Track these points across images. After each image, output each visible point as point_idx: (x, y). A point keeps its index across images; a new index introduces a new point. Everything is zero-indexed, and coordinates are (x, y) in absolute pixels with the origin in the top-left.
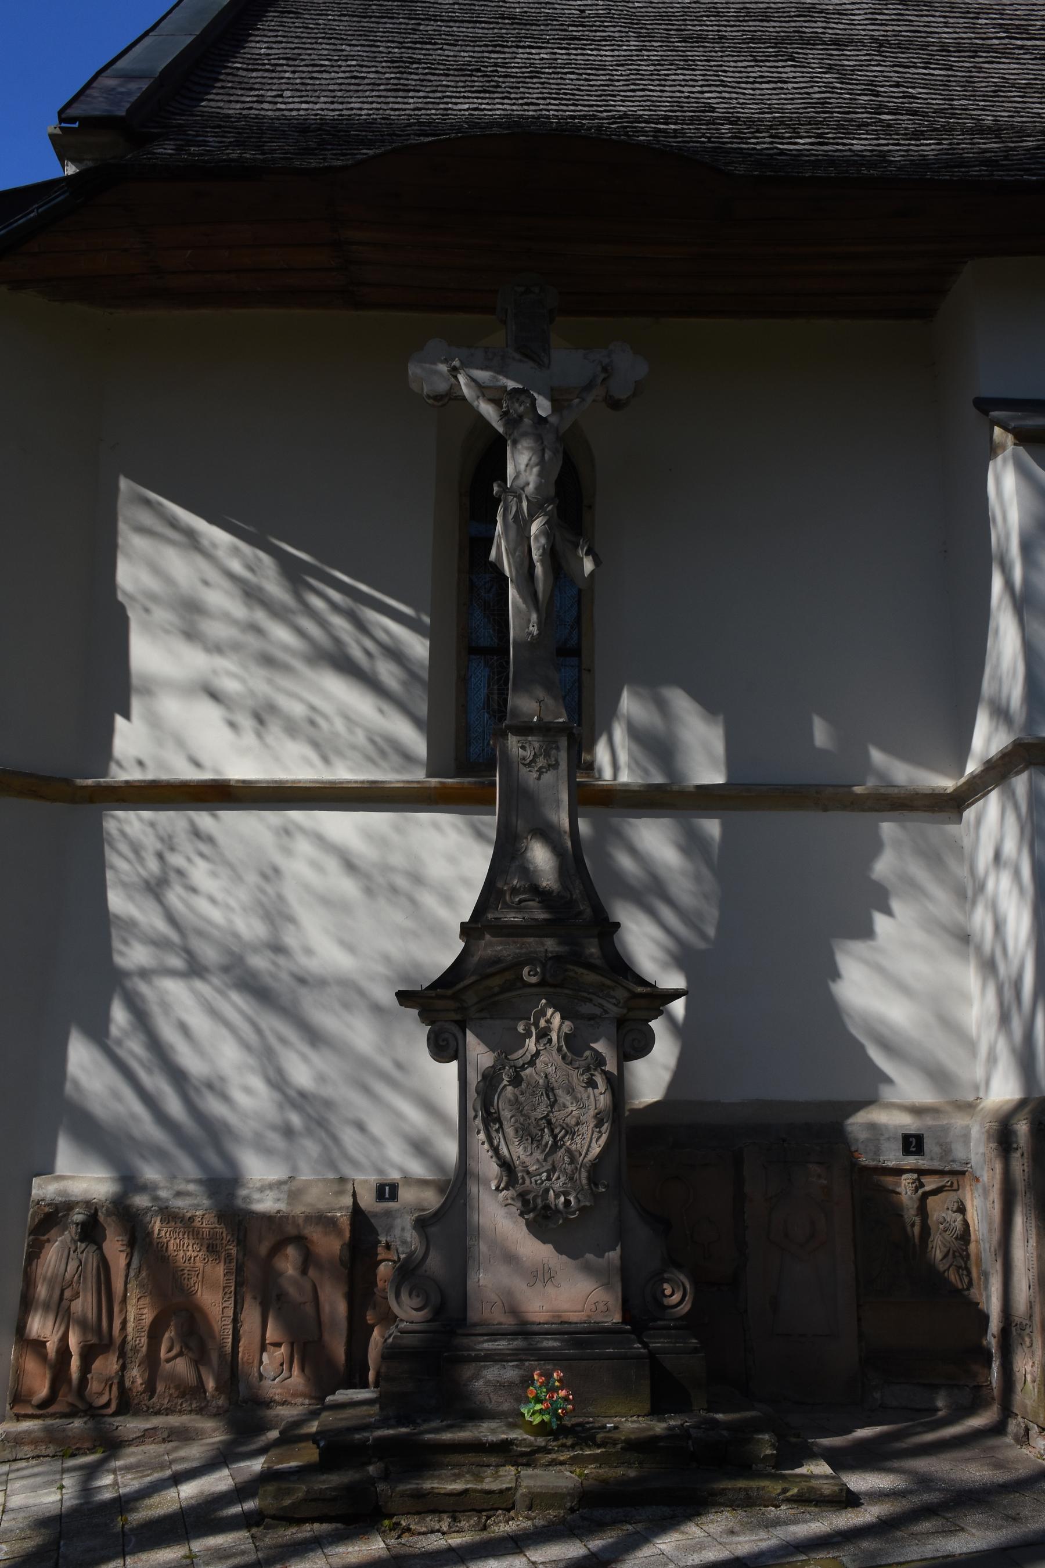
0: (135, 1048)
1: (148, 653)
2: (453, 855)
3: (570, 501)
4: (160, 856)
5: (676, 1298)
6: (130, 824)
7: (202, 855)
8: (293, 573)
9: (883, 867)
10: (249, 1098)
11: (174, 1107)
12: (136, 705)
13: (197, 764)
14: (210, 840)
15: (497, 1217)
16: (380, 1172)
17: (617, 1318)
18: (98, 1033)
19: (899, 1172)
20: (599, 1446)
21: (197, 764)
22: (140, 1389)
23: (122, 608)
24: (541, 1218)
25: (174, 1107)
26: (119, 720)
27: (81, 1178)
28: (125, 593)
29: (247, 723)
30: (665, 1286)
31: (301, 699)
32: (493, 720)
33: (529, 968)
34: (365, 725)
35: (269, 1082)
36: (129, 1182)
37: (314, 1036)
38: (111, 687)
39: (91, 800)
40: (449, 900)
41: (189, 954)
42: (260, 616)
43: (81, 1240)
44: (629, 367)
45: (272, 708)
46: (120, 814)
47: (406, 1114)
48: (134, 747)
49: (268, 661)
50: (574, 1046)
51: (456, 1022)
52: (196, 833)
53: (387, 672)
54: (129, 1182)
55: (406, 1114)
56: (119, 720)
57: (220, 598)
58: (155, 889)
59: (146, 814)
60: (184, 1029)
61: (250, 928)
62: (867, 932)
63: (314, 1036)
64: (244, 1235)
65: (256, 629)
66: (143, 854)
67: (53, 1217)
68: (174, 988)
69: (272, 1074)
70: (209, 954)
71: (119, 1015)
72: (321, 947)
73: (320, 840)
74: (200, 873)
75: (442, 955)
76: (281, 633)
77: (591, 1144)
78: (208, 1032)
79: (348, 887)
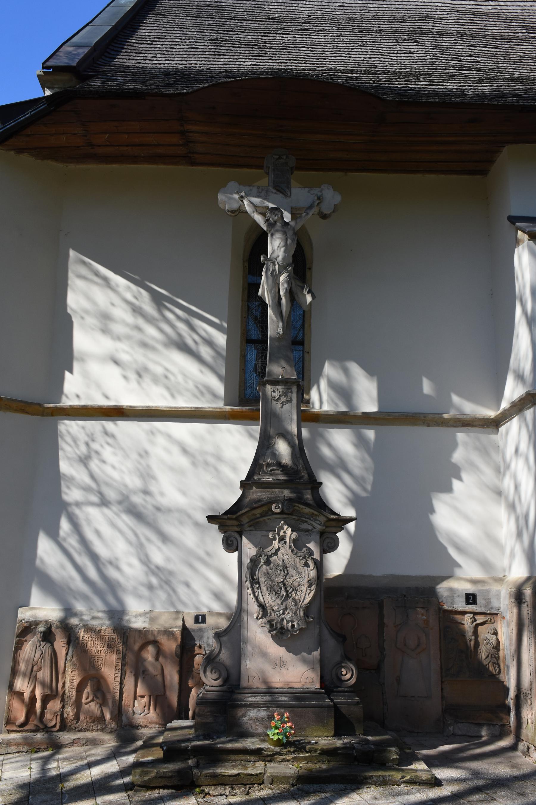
0: (72, 542)
1: (82, 340)
2: (238, 445)
3: (300, 265)
4: (87, 444)
5: (348, 676)
6: (70, 427)
7: (108, 444)
8: (158, 300)
9: (458, 456)
10: (130, 571)
11: (92, 573)
12: (76, 366)
13: (107, 397)
14: (113, 436)
15: (257, 633)
16: (197, 608)
17: (318, 686)
18: (54, 534)
19: (463, 613)
20: (307, 752)
21: (107, 397)
22: (72, 718)
23: (69, 317)
24: (280, 633)
25: (92, 573)
26: (67, 374)
27: (43, 609)
28: (71, 309)
29: (133, 376)
30: (343, 670)
31: (161, 365)
32: (262, 371)
33: (277, 503)
34: (199, 381)
35: (141, 560)
36: (69, 611)
37: (165, 538)
38: (62, 356)
39: (52, 415)
40: (234, 469)
41: (101, 494)
42: (141, 322)
43: (43, 641)
44: (331, 197)
45: (146, 369)
46: (67, 422)
47: (208, 580)
48: (75, 389)
49: (144, 345)
50: (297, 545)
51: (237, 532)
52: (106, 433)
53: (205, 352)
54: (69, 611)
55: (208, 580)
56: (67, 374)
57: (121, 313)
58: (84, 461)
59: (80, 423)
60: (98, 533)
61: (133, 482)
62: (449, 489)
63: (165, 538)
64: (128, 640)
65: (139, 329)
66: (78, 443)
67: (28, 629)
68: (93, 512)
69: (143, 557)
70: (111, 495)
71: (65, 525)
72: (169, 492)
73: (169, 437)
74: (107, 453)
75: (230, 497)
76: (151, 331)
77: (306, 595)
78: (110, 535)
79: (184, 461)
